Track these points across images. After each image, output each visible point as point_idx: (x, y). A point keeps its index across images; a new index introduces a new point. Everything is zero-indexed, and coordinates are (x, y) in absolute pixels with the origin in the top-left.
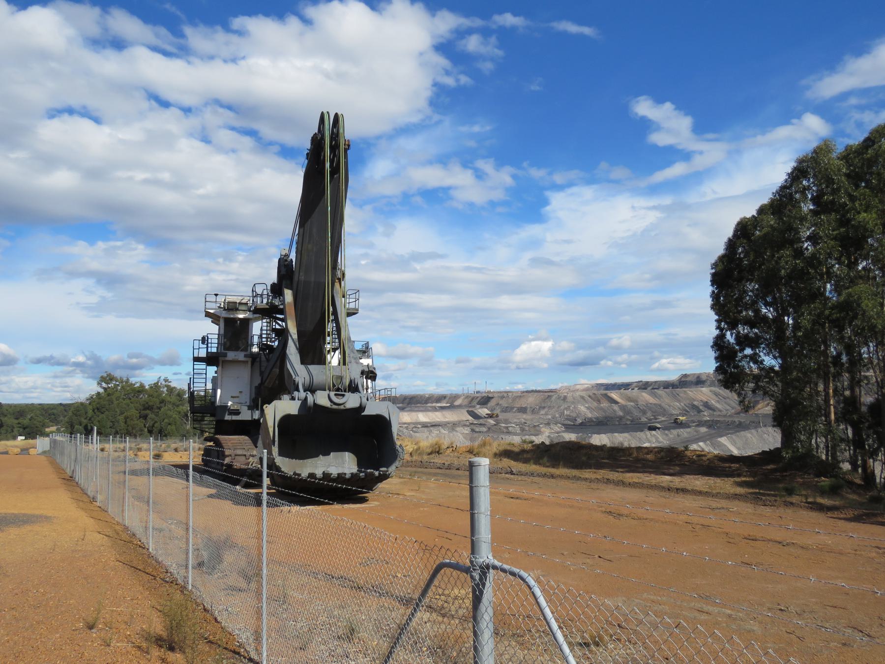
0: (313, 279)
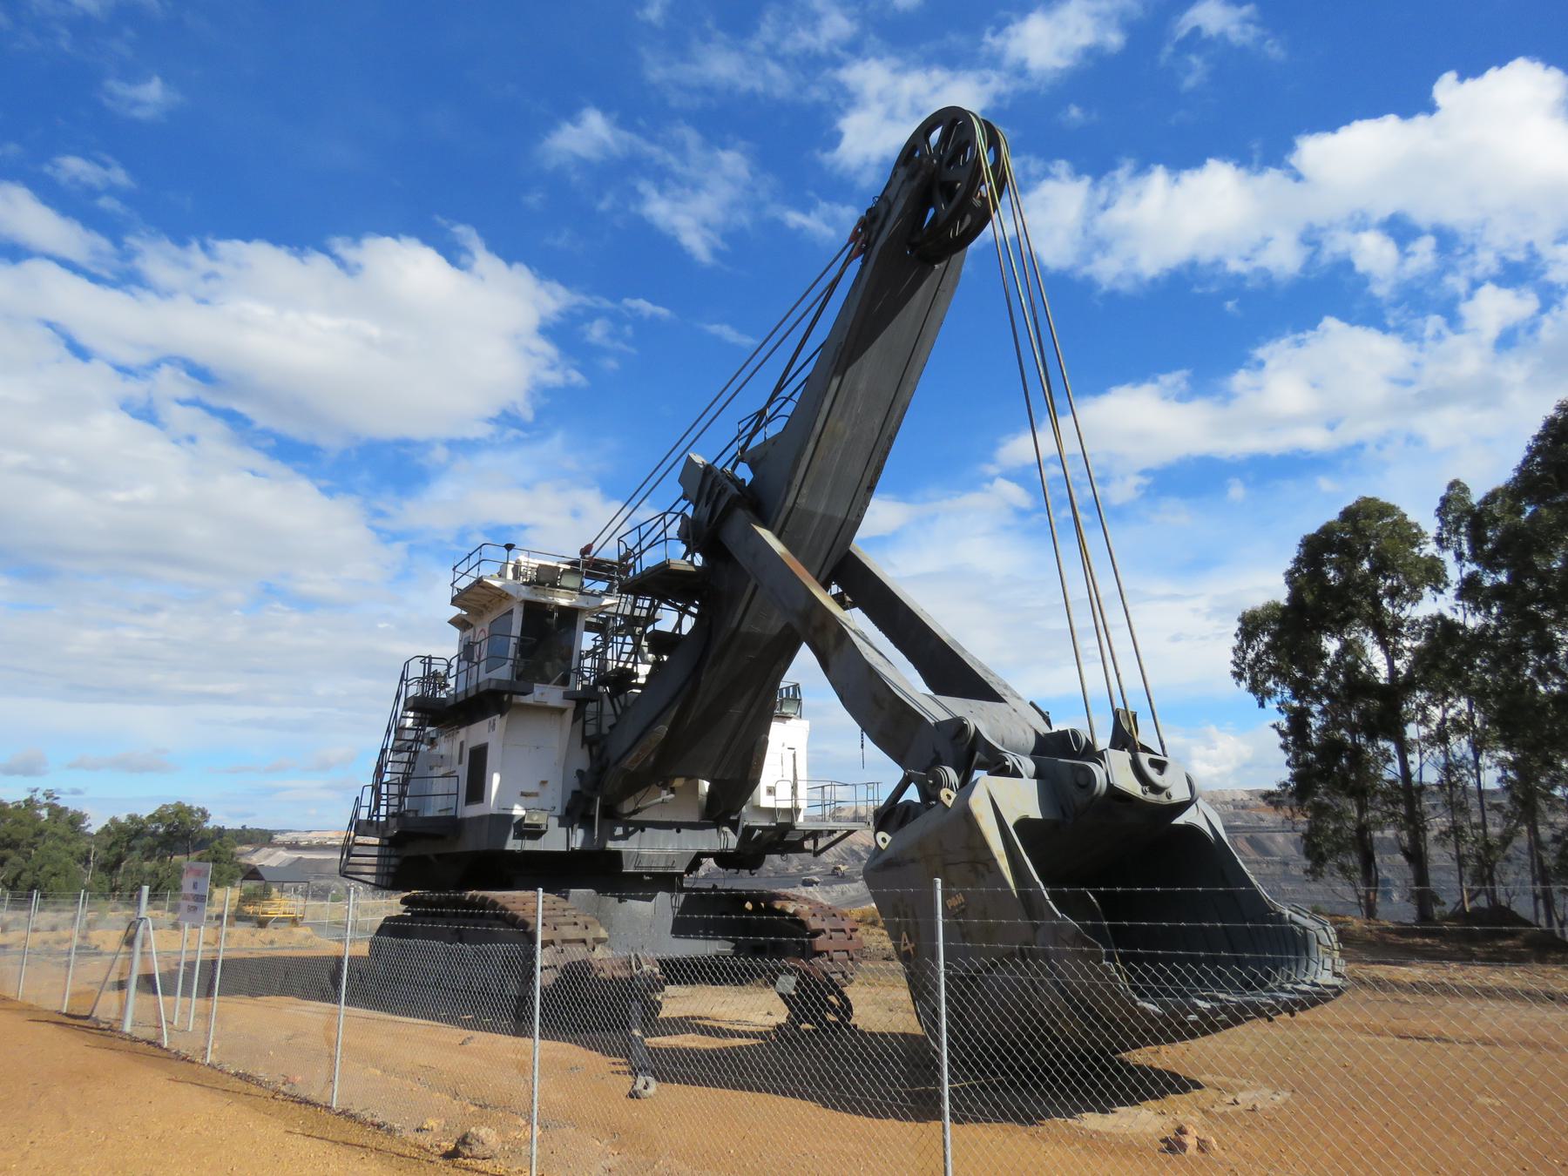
0: (821, 509)
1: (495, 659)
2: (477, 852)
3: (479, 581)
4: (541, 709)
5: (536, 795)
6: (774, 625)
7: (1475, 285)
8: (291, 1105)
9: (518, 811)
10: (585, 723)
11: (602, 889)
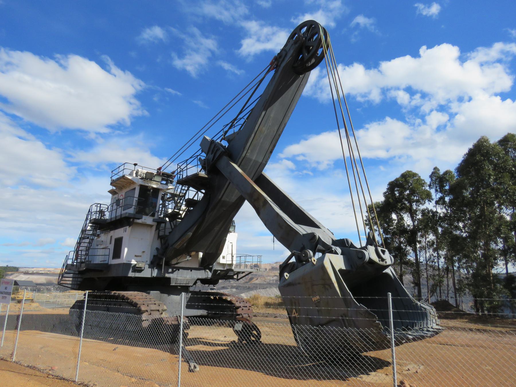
0: (254, 158)
1: (127, 207)
2: (114, 277)
3: (124, 176)
5: (140, 256)
6: (233, 198)
7: (431, 111)
8: (57, 380)
9: (134, 262)
10: (159, 231)
11: (162, 292)
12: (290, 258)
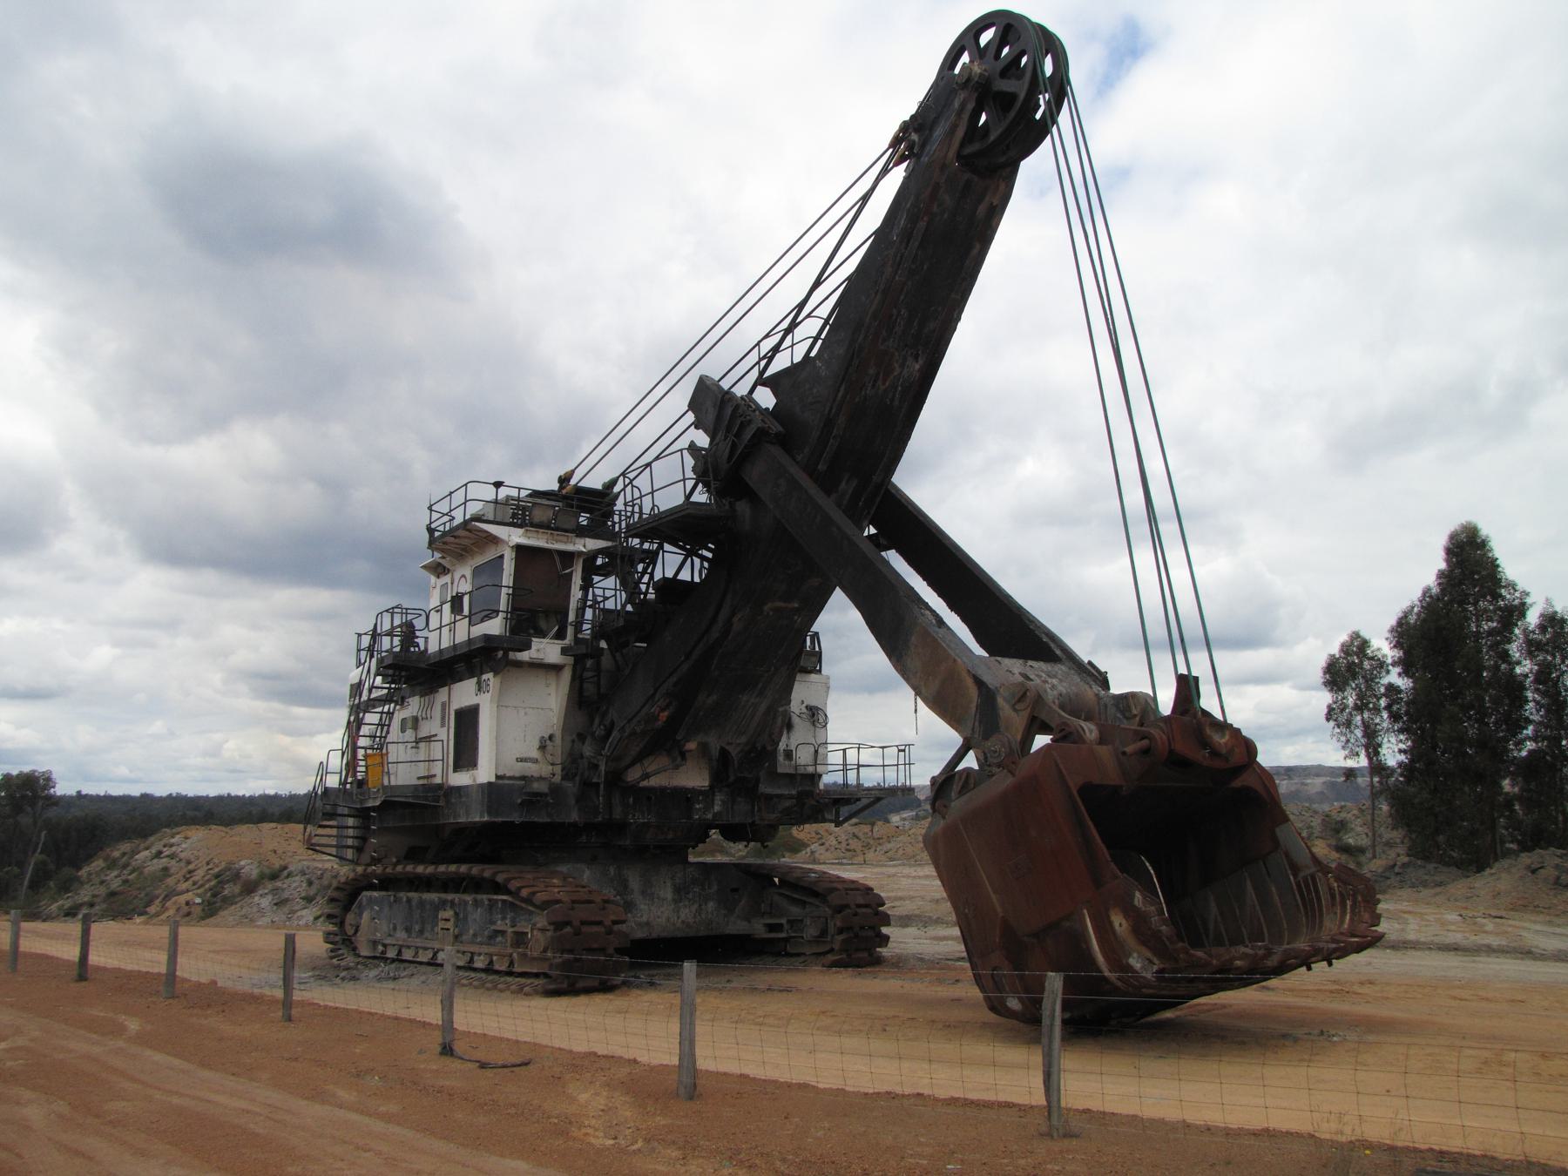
4: (539, 666)
12: (960, 756)
